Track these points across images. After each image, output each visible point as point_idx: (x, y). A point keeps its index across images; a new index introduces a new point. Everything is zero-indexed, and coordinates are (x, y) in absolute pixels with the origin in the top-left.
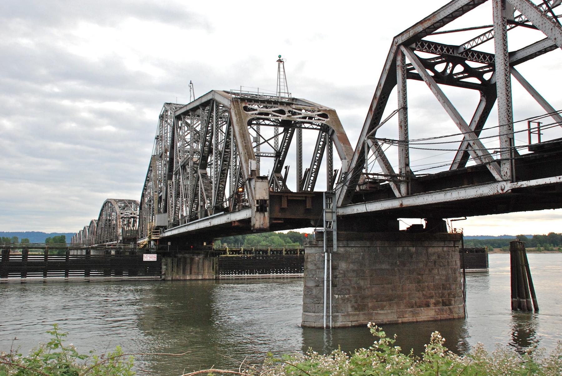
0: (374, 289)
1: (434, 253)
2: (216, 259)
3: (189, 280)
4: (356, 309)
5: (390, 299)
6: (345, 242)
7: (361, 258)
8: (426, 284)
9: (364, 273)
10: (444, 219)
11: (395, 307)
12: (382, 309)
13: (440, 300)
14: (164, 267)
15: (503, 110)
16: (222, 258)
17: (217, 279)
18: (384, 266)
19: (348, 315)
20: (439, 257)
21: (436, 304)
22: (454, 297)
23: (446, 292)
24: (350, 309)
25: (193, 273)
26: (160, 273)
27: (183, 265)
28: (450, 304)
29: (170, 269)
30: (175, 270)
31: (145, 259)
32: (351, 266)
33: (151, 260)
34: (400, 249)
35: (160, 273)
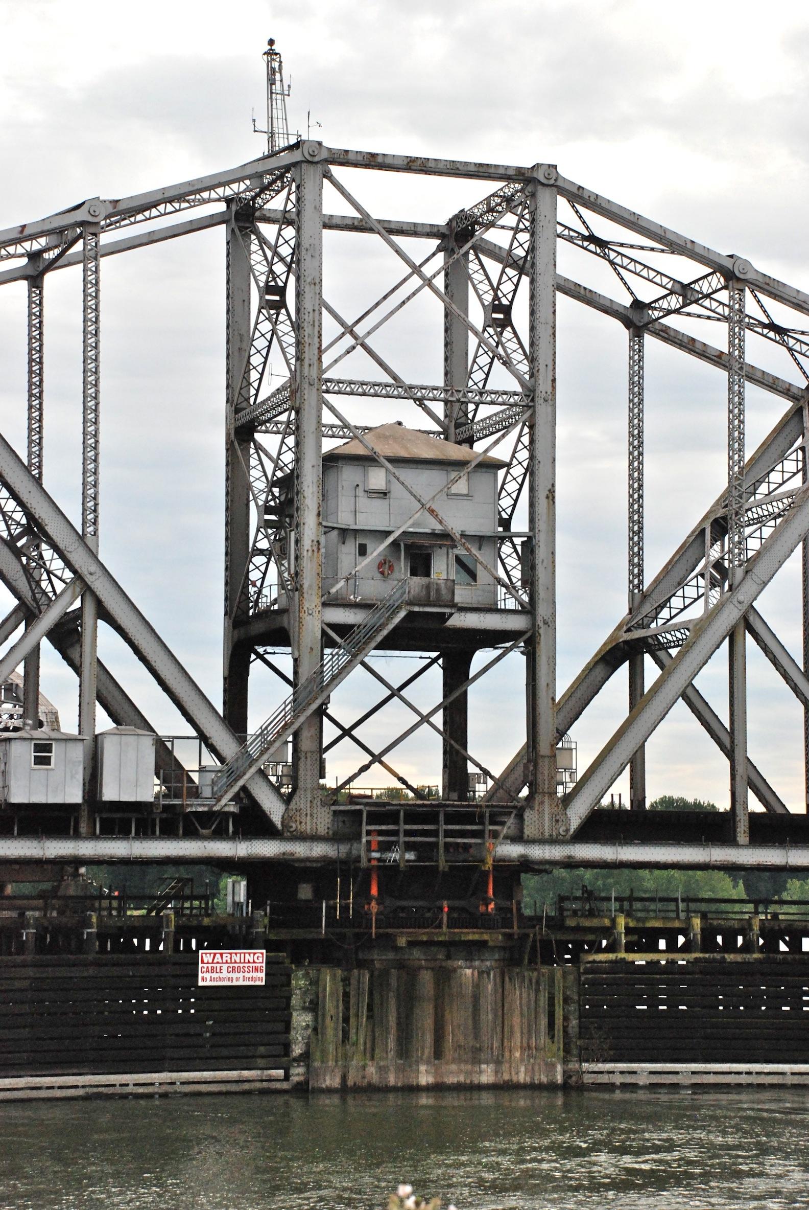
2: (560, 973)
3: (428, 1089)
14: (301, 1019)
16: (595, 969)
17: (571, 1087)
25: (449, 1053)
26: (280, 1054)
27: (397, 1004)
29: (332, 1030)
30: (360, 1035)
31: (205, 979)
33: (240, 980)
35: (280, 1054)
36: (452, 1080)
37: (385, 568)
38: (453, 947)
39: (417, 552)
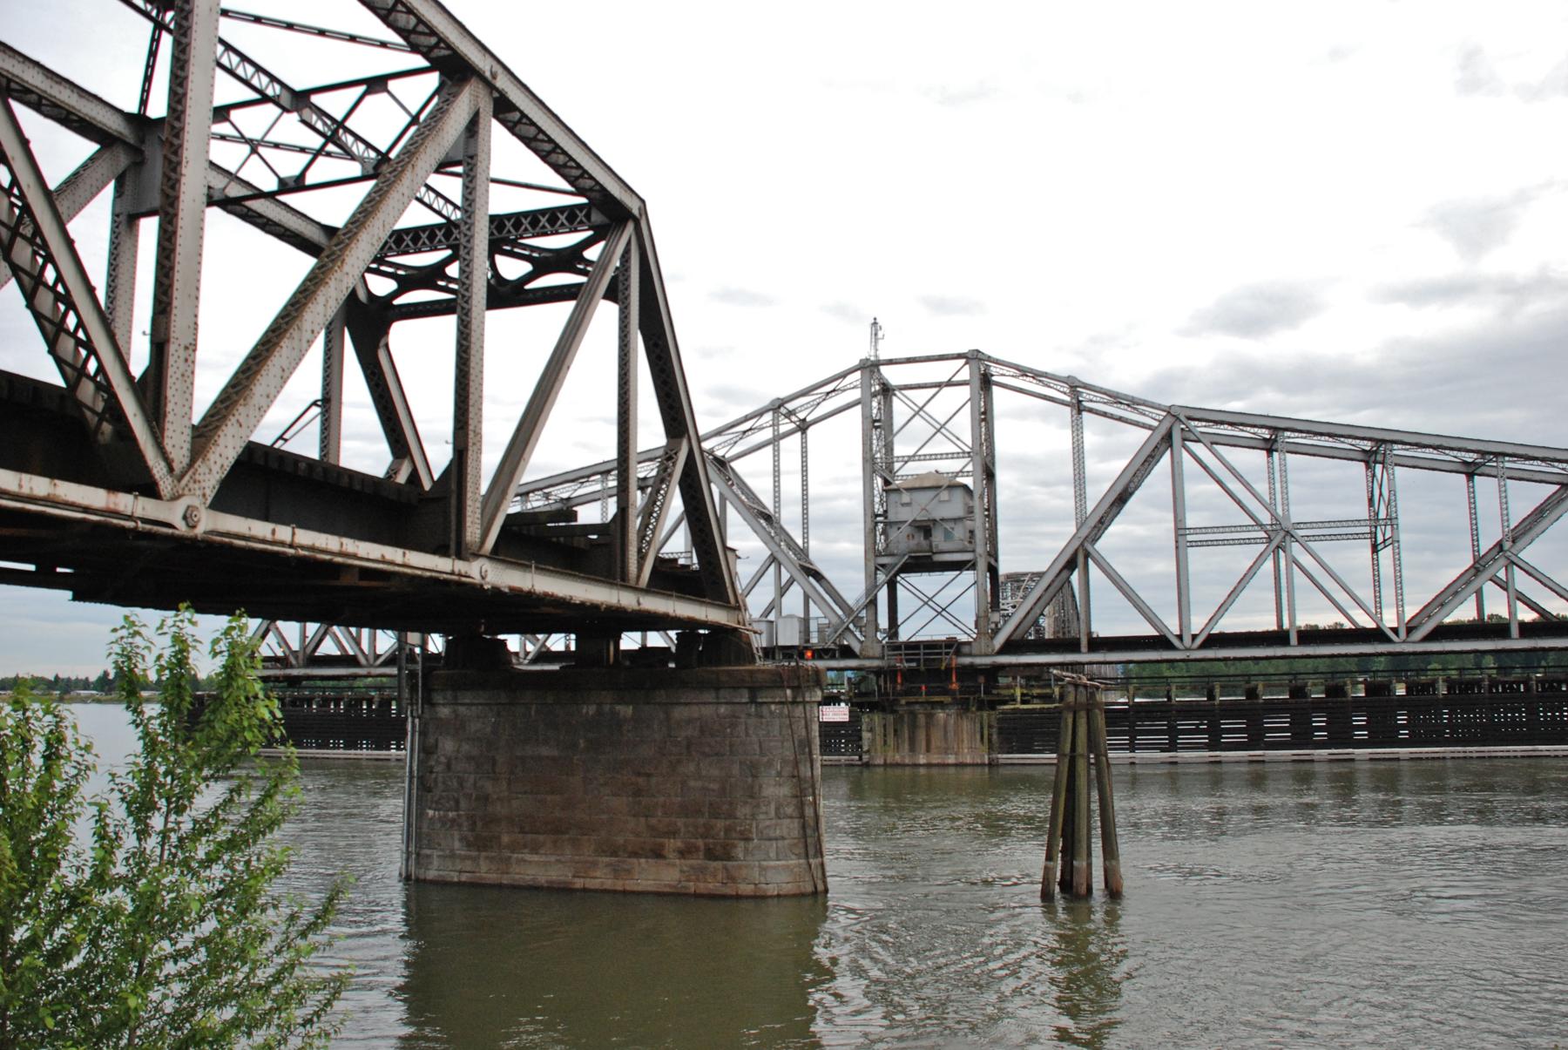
0: (515, 803)
1: (690, 721)
3: (956, 765)
4: (469, 845)
5: (557, 829)
6: (449, 694)
7: (489, 729)
8: (662, 799)
9: (494, 763)
10: (501, 637)
11: (568, 851)
12: (535, 851)
13: (700, 843)
14: (866, 735)
15: (296, 343)
16: (1004, 712)
18: (545, 751)
19: (453, 856)
20: (702, 731)
21: (683, 854)
22: (748, 839)
23: (720, 824)
24: (457, 844)
27: (907, 728)
28: (730, 858)
29: (879, 739)
30: (891, 740)
32: (466, 747)
33: (838, 719)
34: (591, 710)
36: (935, 762)
37: (911, 536)
38: (934, 705)
39: (925, 528)
